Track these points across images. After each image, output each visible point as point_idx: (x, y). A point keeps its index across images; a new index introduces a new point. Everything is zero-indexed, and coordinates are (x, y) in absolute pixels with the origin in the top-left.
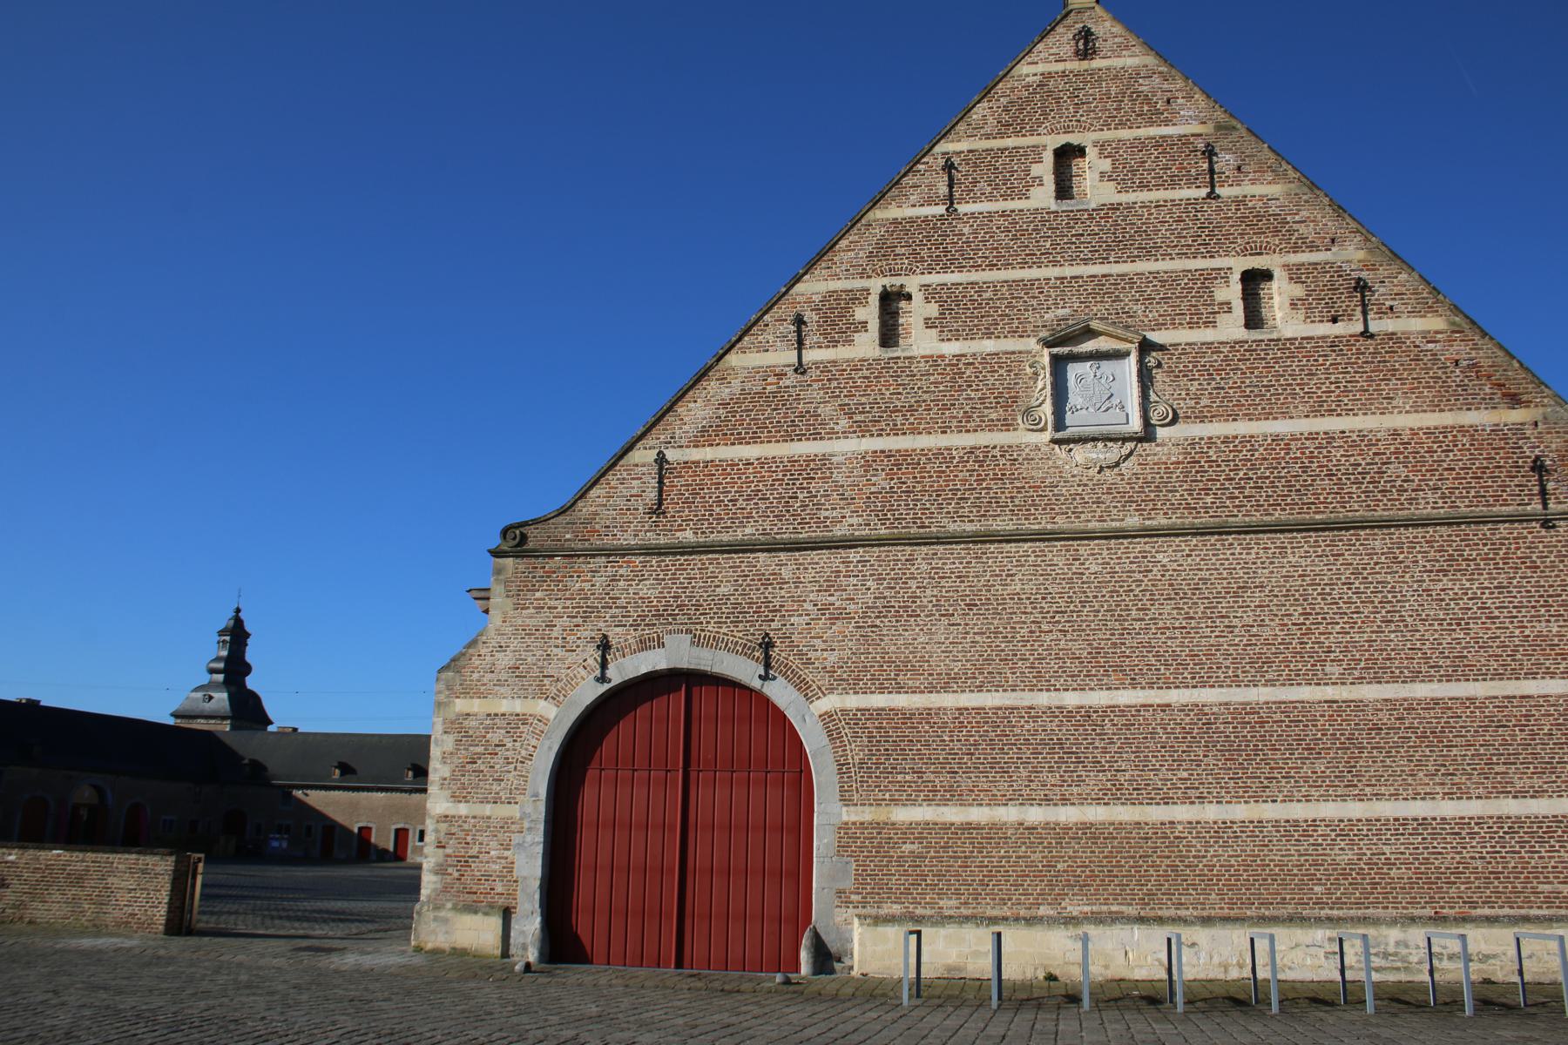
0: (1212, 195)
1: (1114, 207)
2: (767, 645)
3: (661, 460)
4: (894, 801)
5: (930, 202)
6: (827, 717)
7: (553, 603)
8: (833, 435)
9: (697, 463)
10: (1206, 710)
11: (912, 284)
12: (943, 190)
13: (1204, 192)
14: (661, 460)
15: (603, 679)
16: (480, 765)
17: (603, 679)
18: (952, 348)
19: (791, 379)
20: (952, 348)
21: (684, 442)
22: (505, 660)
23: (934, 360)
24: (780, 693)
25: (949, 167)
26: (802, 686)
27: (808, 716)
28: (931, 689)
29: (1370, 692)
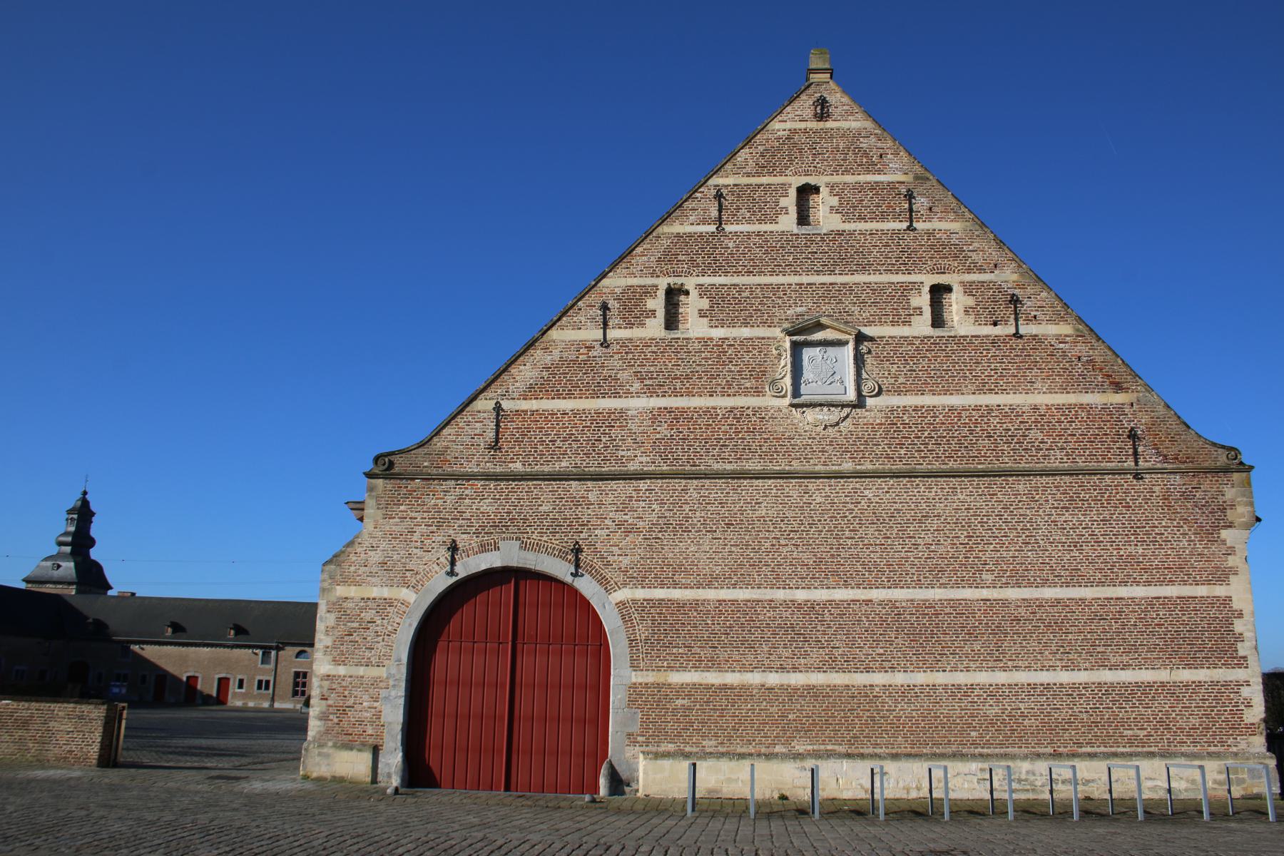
0: (910, 228)
1: (840, 233)
2: (577, 551)
3: (498, 408)
6: (621, 605)
7: (413, 515)
8: (628, 394)
11: (690, 283)
12: (715, 213)
14: (498, 408)
15: (451, 573)
17: (451, 573)
18: (718, 333)
23: (705, 341)
24: (586, 586)
25: (719, 196)
26: (603, 581)
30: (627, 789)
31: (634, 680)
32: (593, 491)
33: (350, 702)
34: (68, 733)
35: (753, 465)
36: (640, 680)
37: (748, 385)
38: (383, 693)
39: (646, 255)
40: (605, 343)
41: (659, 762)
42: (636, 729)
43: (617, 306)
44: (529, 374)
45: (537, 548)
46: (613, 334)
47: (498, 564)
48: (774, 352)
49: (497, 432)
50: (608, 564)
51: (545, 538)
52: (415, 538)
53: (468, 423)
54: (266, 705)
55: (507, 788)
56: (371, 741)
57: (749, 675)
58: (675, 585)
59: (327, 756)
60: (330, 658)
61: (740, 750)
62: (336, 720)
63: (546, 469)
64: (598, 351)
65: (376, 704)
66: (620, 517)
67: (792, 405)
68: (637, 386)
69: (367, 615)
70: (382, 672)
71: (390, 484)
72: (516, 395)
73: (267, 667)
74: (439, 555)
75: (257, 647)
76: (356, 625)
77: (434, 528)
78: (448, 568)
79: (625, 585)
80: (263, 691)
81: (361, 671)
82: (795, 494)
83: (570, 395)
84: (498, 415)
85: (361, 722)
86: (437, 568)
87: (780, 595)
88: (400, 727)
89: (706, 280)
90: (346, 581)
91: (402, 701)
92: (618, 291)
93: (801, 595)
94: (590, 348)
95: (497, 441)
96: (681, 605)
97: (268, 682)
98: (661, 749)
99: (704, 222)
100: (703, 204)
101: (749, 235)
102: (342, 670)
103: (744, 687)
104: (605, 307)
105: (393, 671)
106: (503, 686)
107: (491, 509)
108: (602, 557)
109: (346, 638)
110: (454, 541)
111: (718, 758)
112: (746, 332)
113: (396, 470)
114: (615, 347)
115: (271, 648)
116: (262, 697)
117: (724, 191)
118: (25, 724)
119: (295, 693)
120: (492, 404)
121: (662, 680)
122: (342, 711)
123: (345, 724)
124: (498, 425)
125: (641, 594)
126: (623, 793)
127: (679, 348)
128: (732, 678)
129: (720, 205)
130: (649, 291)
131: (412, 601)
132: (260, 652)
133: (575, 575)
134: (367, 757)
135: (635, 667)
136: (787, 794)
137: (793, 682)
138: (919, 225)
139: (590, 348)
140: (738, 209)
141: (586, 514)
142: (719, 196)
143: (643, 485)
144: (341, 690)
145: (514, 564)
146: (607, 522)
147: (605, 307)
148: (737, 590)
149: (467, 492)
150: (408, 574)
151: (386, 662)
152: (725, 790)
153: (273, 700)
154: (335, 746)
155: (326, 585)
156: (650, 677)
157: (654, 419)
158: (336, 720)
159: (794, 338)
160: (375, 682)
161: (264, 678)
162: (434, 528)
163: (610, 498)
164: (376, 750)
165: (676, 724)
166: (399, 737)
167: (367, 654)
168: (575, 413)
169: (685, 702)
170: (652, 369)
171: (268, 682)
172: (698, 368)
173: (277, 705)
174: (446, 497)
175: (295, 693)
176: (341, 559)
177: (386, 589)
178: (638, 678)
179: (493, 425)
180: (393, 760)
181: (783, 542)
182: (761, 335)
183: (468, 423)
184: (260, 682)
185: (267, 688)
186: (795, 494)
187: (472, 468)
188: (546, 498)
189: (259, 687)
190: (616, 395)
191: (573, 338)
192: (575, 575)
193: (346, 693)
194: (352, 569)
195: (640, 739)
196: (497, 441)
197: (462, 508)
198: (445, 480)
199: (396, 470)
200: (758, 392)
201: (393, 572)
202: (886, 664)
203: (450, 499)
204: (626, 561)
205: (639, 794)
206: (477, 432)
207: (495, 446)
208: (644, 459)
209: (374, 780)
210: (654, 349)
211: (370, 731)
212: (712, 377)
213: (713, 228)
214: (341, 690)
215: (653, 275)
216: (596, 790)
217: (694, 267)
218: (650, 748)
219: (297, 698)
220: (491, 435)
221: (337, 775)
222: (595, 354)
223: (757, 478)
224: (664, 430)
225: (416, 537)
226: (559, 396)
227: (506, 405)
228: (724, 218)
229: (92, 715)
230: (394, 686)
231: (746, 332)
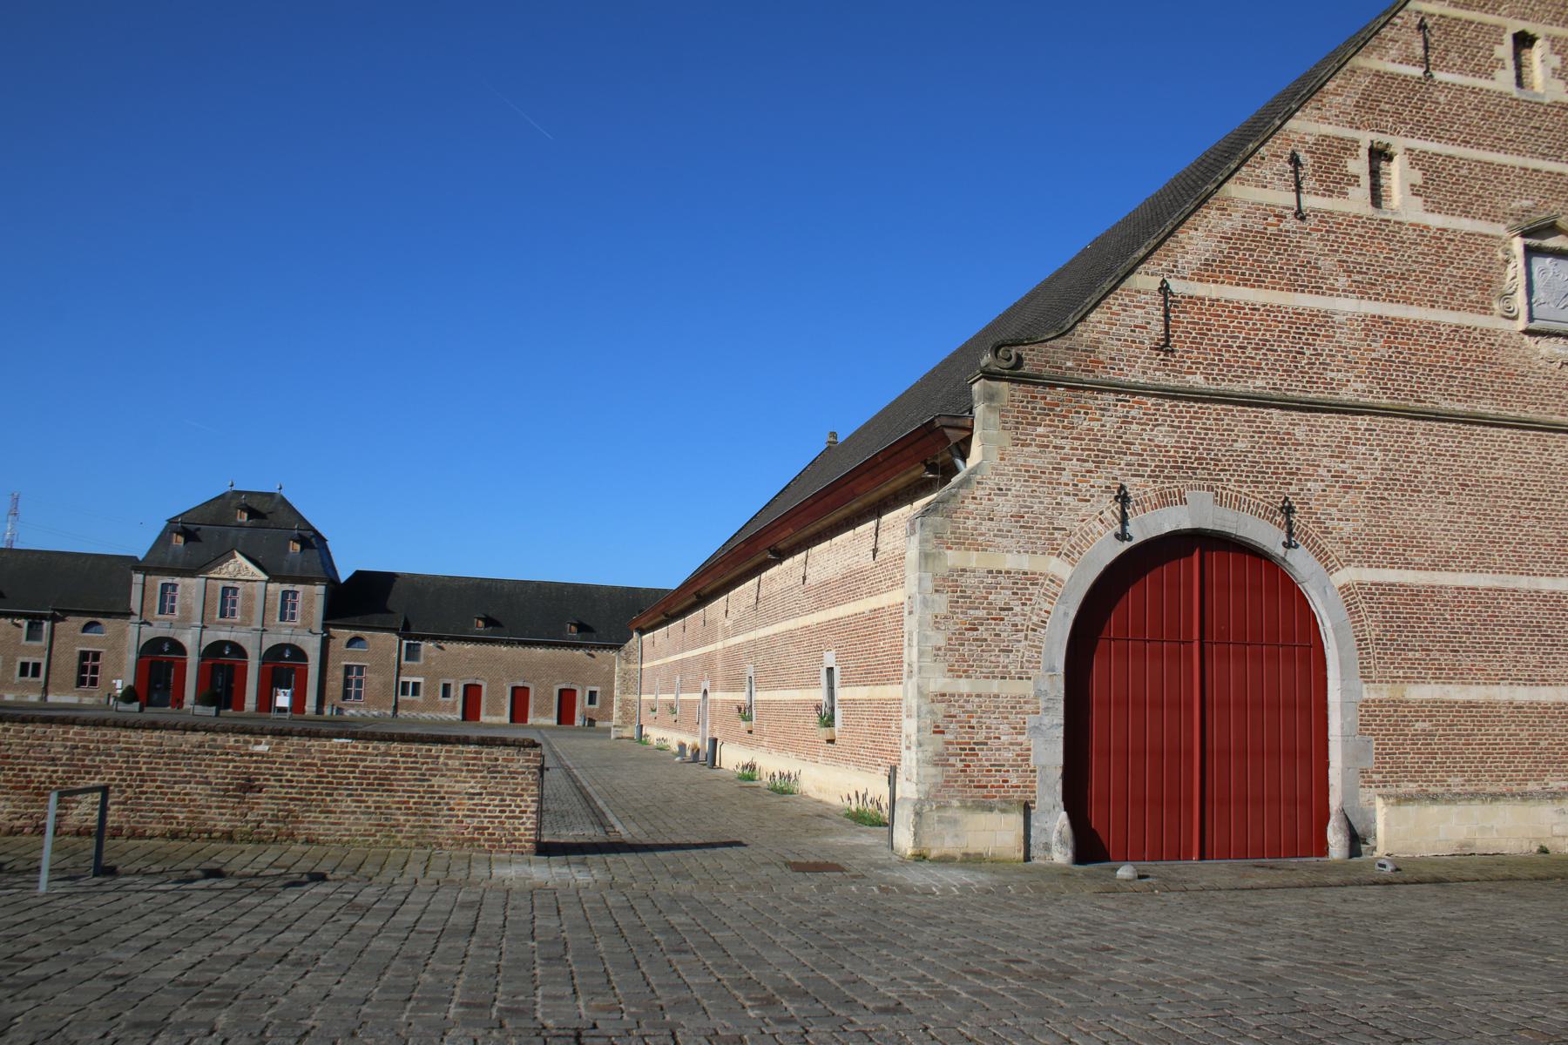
2: (1288, 510)
3: (1164, 289)
7: (1058, 442)
11: (1398, 144)
12: (1420, 52)
14: (1164, 289)
17: (1122, 536)
18: (1436, 221)
24: (1301, 563)
25: (1422, 27)
26: (1322, 556)
30: (1364, 847)
31: (1366, 696)
32: (1299, 426)
33: (980, 737)
34: (472, 796)
35: (1485, 407)
36: (1373, 696)
37: (1473, 297)
38: (1031, 720)
39: (1340, 93)
40: (1300, 215)
41: (1403, 808)
42: (1370, 763)
43: (1311, 161)
44: (1201, 245)
45: (1237, 502)
46: (1309, 202)
47: (1186, 524)
48: (1501, 255)
49: (1167, 326)
50: (1327, 532)
51: (1245, 490)
52: (1063, 480)
53: (1125, 308)
54: (34, 698)
55: (1202, 857)
56: (1017, 795)
57: (1496, 688)
58: (1408, 565)
59: (955, 822)
60: (944, 666)
61: (1489, 789)
62: (960, 765)
63: (1237, 388)
64: (1291, 224)
65: (1021, 738)
66: (1336, 465)
67: (1527, 332)
68: (1343, 282)
69: (1000, 598)
70: (1026, 688)
71: (1019, 391)
72: (1187, 273)
73: (36, 644)
74: (1102, 507)
75: (21, 616)
76: (982, 613)
77: (1090, 465)
78: (1117, 528)
79: (1349, 562)
80: (29, 679)
81: (995, 686)
82: (1532, 449)
83: (1259, 283)
84: (1166, 300)
85: (999, 766)
86: (1100, 527)
87: (1524, 583)
88: (1060, 772)
89: (1418, 144)
90: (963, 542)
91: (1060, 732)
92: (1310, 140)
93: (1546, 584)
94: (1281, 217)
95: (1167, 338)
96: (1415, 593)
97: (37, 666)
98: (1401, 791)
99: (1406, 60)
100: (1405, 35)
101: (1462, 89)
102: (964, 686)
104: (1295, 160)
105: (1045, 686)
106: (1190, 706)
107: (1170, 441)
108: (1319, 522)
109: (969, 634)
110: (1122, 487)
111: (1448, 802)
112: (1466, 224)
113: (1026, 369)
114: (1312, 222)
115: (43, 617)
116: (27, 687)
117: (1429, 22)
118: (383, 782)
119: (81, 682)
120: (1155, 283)
121: (1398, 696)
122: (970, 751)
123: (974, 771)
124: (1166, 316)
125: (1370, 575)
126: (1359, 854)
127: (1388, 231)
128: (1477, 693)
129: (1426, 41)
130: (1349, 147)
131: (1066, 578)
132: (25, 623)
133: (1288, 545)
134: (1016, 819)
135: (1366, 678)
136: (1547, 845)
137: (1543, 699)
139: (1281, 217)
140: (1447, 50)
141: (1295, 458)
142: (1422, 27)
143: (1362, 422)
144: (964, 717)
145: (1208, 525)
146: (1321, 471)
147: (1295, 160)
148: (1477, 575)
149: (1133, 413)
150: (1057, 534)
151: (1032, 673)
152: (1478, 843)
153: (45, 691)
154: (964, 806)
155: (929, 547)
156: (1385, 692)
157: (1367, 330)
158: (960, 765)
159: (1528, 241)
160: (1017, 704)
161: (31, 660)
162: (1090, 465)
163: (1322, 439)
164: (1027, 809)
165: (1425, 754)
166: (1059, 788)
167: (1003, 659)
168: (1269, 310)
169: (1426, 725)
170: (1360, 259)
171: (37, 666)
172: (1415, 266)
173: (51, 698)
174: (1103, 418)
175: (81, 682)
176: (952, 505)
177: (1025, 557)
178: (1369, 692)
179: (1159, 314)
180: (1055, 823)
181: (1524, 513)
182: (1485, 231)
183: (1125, 308)
184: (24, 666)
185: (36, 673)
186: (1532, 449)
187: (1135, 376)
188: (1240, 432)
189: (24, 672)
190: (1317, 290)
191: (1258, 199)
192: (1288, 545)
193: (974, 722)
194: (970, 523)
195: (1375, 777)
196: (1167, 338)
198: (1100, 391)
199: (1026, 369)
200: (1486, 310)
203: (1110, 422)
204: (1348, 528)
205: (1376, 854)
206: (1139, 322)
207: (1165, 346)
208: (1360, 386)
209: (1027, 858)
210: (1362, 231)
211: (1014, 782)
212: (1432, 282)
213: (1418, 72)
214: (964, 717)
216: (1323, 849)
218: (1390, 790)
219: (83, 688)
220: (1159, 328)
221: (971, 851)
222: (1288, 227)
223: (1492, 425)
224: (1380, 349)
225: (1066, 477)
226: (1244, 282)
227: (1176, 286)
228: (1432, 59)
229: (515, 766)
230: (1046, 709)
231: (1466, 224)
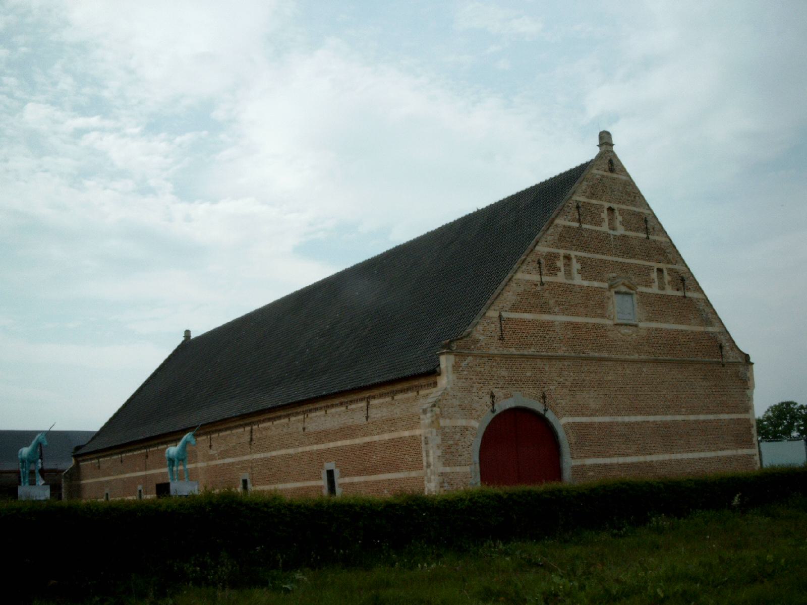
0: (648, 238)
1: (624, 236)
2: (544, 397)
3: (500, 316)
4: (585, 457)
5: (573, 221)
6: (564, 425)
7: (471, 377)
8: (555, 313)
9: (512, 319)
10: (657, 423)
11: (573, 254)
12: (577, 217)
13: (645, 236)
14: (500, 316)
15: (493, 411)
16: (453, 449)
17: (493, 411)
18: (586, 283)
19: (539, 288)
20: (586, 283)
21: (507, 309)
22: (456, 402)
23: (581, 287)
24: (550, 415)
25: (578, 207)
26: (556, 413)
27: (561, 422)
28: (591, 415)
29: (692, 418)
103: (612, 465)
120: (496, 314)
138: (651, 237)
147: (539, 263)
197: (493, 373)
201: (467, 410)
202: (656, 451)
215: (557, 247)
217: (560, 285)
225: (475, 390)
